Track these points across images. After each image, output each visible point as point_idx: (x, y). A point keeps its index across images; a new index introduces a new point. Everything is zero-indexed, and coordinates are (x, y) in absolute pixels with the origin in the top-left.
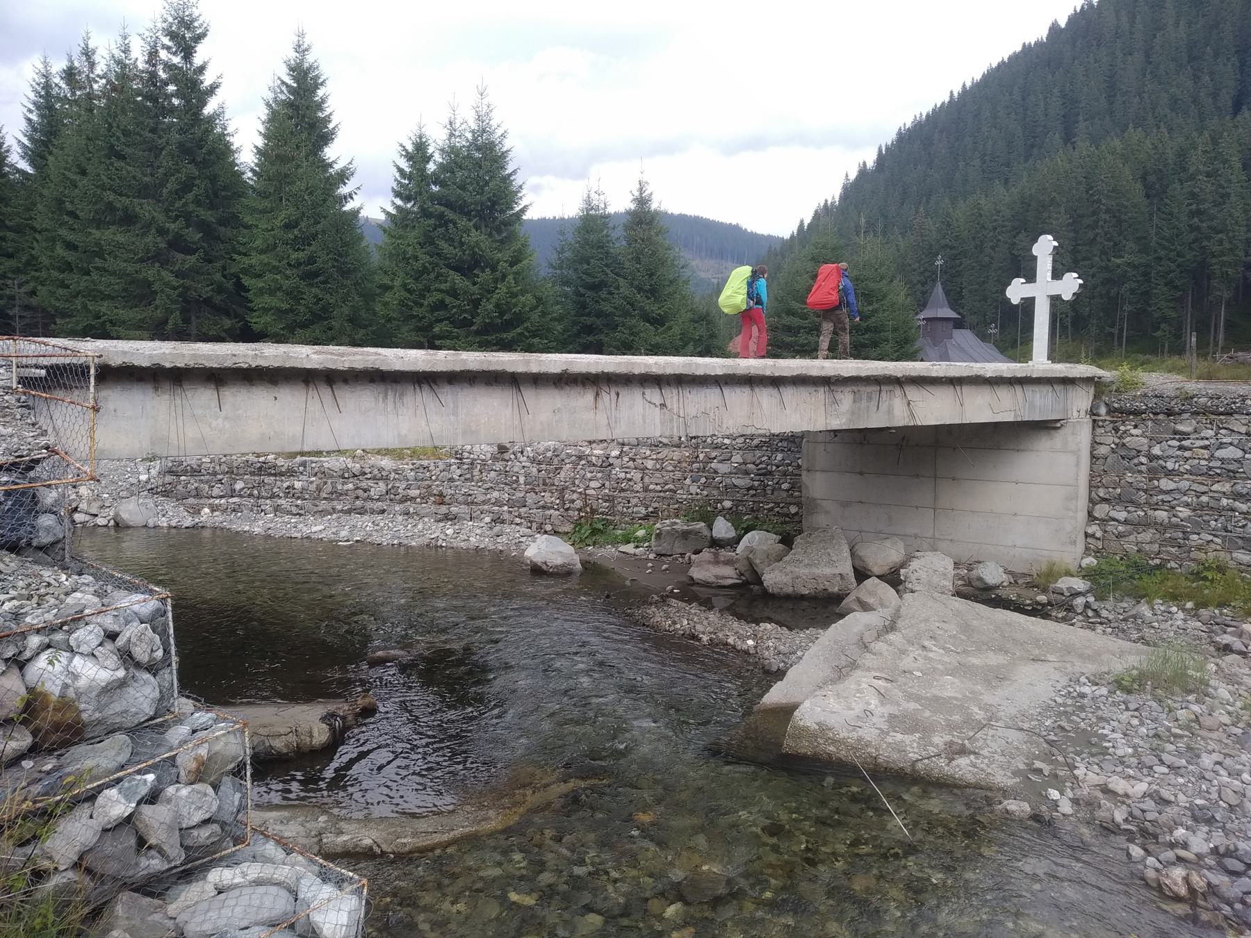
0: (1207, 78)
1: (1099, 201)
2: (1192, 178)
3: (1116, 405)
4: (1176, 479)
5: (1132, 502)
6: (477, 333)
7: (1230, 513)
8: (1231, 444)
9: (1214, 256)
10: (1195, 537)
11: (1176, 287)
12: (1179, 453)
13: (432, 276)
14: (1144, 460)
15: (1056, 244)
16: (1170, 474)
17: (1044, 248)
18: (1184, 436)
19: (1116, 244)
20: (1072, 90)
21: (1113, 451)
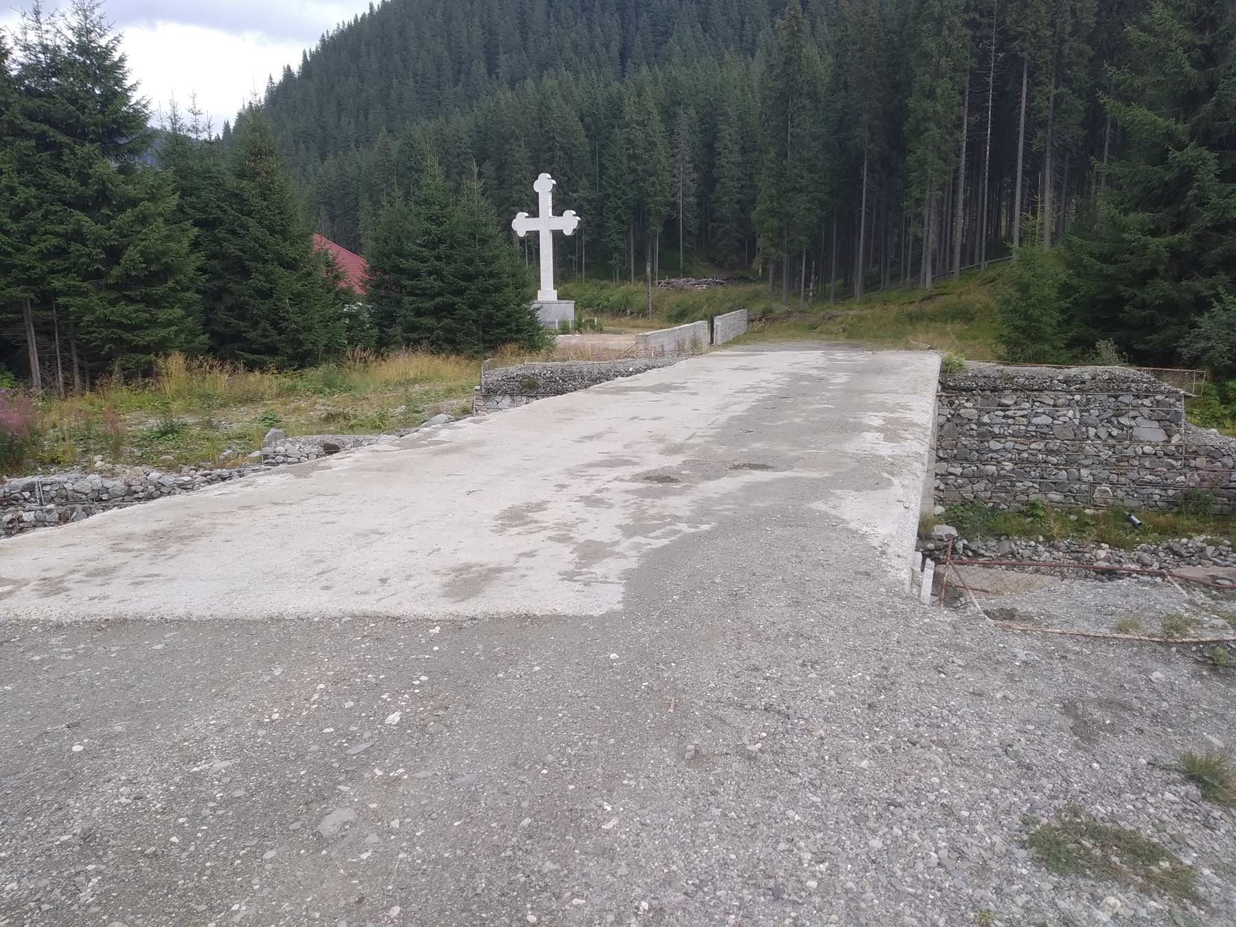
0: (599, 30)
1: (553, 138)
2: (627, 125)
3: (951, 384)
4: (1003, 441)
5: (966, 459)
6: (110, 287)
7: (1044, 465)
8: (1044, 413)
9: (649, 196)
10: (1020, 484)
11: (623, 222)
12: (1003, 421)
13: (39, 214)
14: (974, 427)
15: (554, 182)
16: (995, 436)
17: (544, 185)
18: (1005, 407)
19: (569, 179)
20: (489, 22)
21: (948, 420)
